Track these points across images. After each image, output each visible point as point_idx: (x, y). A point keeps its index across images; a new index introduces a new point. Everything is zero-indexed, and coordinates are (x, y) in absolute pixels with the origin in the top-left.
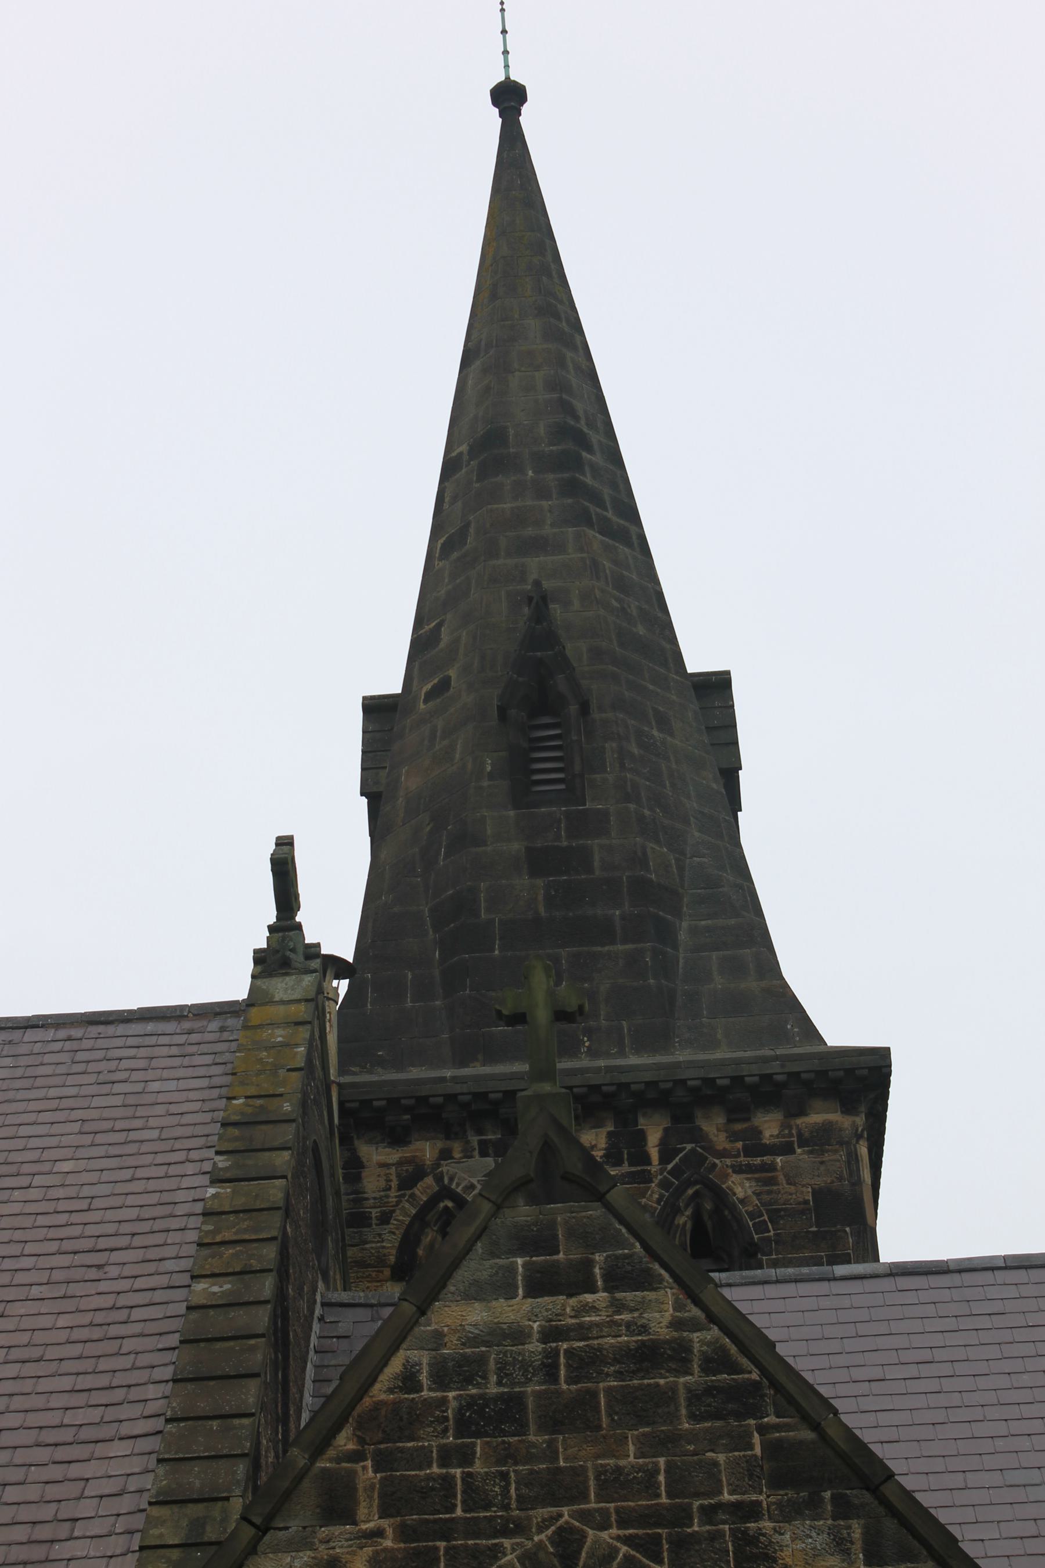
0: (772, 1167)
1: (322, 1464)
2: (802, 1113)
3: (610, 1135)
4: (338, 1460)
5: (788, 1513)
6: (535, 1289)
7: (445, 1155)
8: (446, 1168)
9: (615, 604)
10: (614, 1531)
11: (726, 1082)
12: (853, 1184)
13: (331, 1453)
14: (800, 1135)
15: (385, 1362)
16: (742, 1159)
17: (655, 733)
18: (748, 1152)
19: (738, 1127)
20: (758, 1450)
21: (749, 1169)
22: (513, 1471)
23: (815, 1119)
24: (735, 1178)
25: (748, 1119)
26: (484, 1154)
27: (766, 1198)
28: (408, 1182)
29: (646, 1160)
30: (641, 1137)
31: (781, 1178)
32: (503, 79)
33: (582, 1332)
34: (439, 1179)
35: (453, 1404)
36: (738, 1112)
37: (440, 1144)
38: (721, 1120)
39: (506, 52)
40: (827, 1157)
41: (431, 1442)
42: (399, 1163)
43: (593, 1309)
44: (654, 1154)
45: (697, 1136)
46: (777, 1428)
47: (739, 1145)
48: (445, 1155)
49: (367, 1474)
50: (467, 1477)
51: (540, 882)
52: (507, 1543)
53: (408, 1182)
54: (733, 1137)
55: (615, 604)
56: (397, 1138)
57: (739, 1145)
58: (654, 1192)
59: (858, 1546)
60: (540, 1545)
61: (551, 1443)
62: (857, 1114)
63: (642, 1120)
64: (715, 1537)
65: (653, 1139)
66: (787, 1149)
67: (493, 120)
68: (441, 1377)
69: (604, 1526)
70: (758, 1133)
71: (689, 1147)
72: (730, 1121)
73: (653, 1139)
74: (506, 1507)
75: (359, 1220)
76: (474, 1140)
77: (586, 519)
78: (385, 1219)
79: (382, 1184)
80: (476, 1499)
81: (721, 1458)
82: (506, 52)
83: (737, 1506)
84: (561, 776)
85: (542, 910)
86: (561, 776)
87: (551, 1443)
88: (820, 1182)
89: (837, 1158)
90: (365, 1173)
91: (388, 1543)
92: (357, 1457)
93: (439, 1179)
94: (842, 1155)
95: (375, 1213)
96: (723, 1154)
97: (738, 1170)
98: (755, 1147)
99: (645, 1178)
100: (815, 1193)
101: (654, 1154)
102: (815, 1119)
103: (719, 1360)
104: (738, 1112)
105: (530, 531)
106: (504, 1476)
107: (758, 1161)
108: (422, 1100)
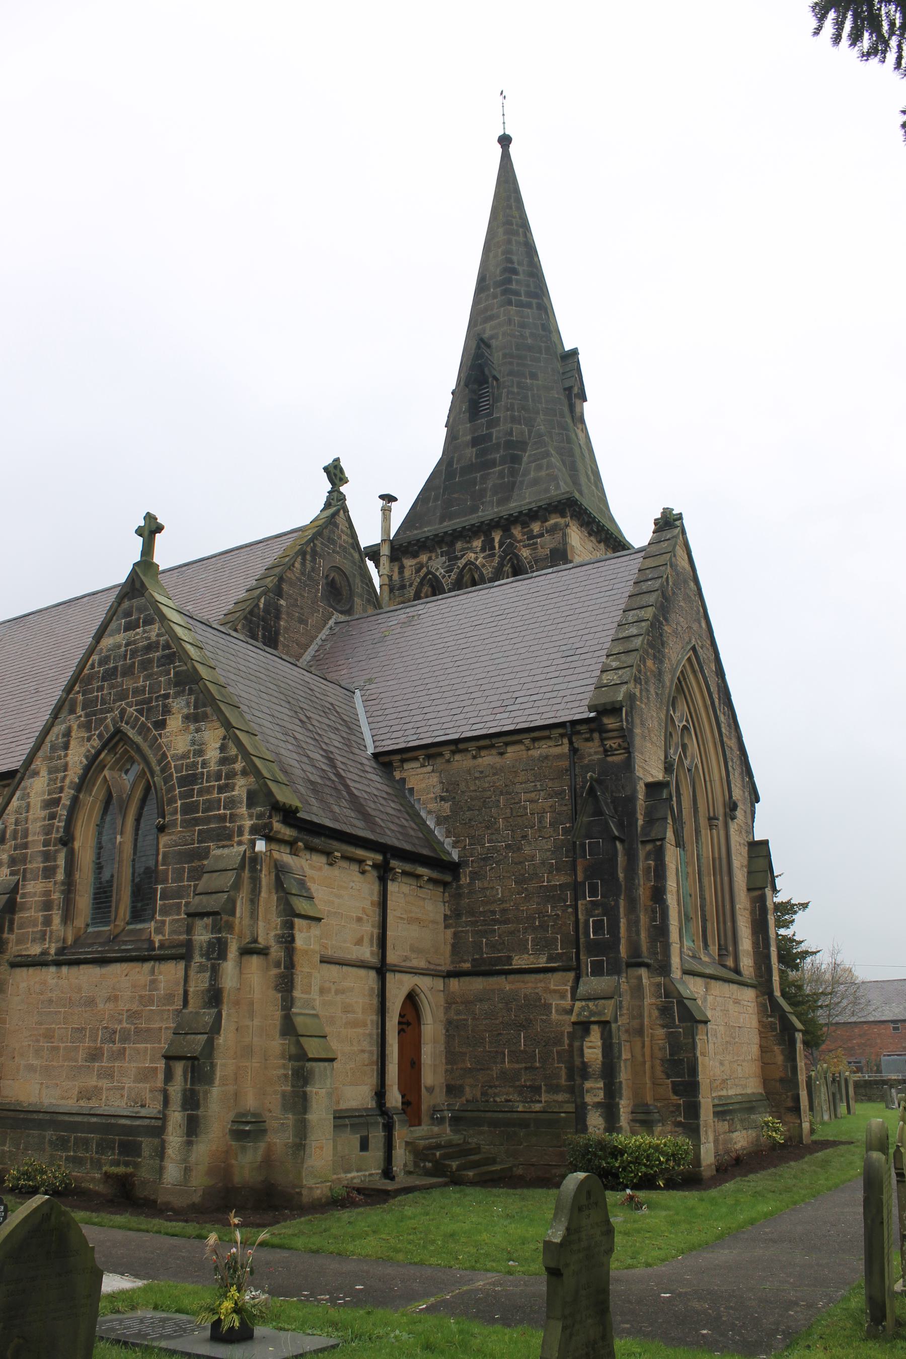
0: (536, 543)
1: (71, 696)
2: (546, 521)
3: (482, 541)
4: (74, 694)
5: (177, 695)
6: (127, 629)
7: (430, 559)
8: (430, 563)
9: (517, 333)
10: (134, 708)
11: (516, 514)
12: (564, 545)
13: (73, 692)
14: (546, 529)
15: (88, 661)
16: (527, 542)
17: (528, 381)
18: (529, 539)
19: (525, 530)
20: (172, 675)
21: (529, 545)
22: (112, 691)
23: (552, 522)
24: (524, 550)
25: (529, 527)
26: (442, 556)
27: (533, 555)
28: (418, 571)
29: (494, 548)
30: (493, 540)
31: (539, 547)
32: (502, 133)
33: (134, 643)
34: (428, 568)
35: (102, 672)
36: (525, 525)
37: (428, 555)
38: (520, 529)
39: (504, 123)
40: (555, 536)
41: (95, 685)
42: (416, 564)
43: (138, 634)
44: (497, 545)
45: (511, 536)
46: (178, 666)
47: (526, 537)
48: (430, 559)
49: (80, 697)
50: (102, 694)
51: (474, 449)
52: (108, 715)
53: (418, 571)
54: (524, 534)
55: (517, 333)
56: (415, 555)
57: (526, 537)
58: (497, 559)
59: (192, 704)
60: (116, 715)
61: (123, 681)
62: (566, 517)
63: (493, 534)
64: (158, 706)
65: (497, 540)
66: (541, 535)
67: (498, 150)
68: (100, 665)
69: (131, 707)
70: (532, 531)
71: (508, 541)
72: (523, 528)
73: (497, 540)
74: (110, 704)
75: (403, 587)
76: (439, 551)
77: (510, 303)
78: (411, 585)
79: (410, 573)
80: (104, 702)
81: (163, 679)
82: (504, 123)
83: (164, 695)
84: (488, 407)
85: (474, 461)
86: (488, 407)
87: (123, 681)
88: (552, 546)
89: (558, 536)
90: (405, 570)
91: (82, 719)
92: (78, 692)
93: (428, 568)
94: (561, 533)
95: (408, 584)
96: (519, 542)
97: (525, 546)
98: (531, 537)
99: (493, 555)
100: (550, 551)
101: (497, 545)
102: (552, 522)
103: (167, 646)
104: (525, 525)
105: (489, 313)
106: (110, 693)
107: (531, 542)
108: (418, 540)
